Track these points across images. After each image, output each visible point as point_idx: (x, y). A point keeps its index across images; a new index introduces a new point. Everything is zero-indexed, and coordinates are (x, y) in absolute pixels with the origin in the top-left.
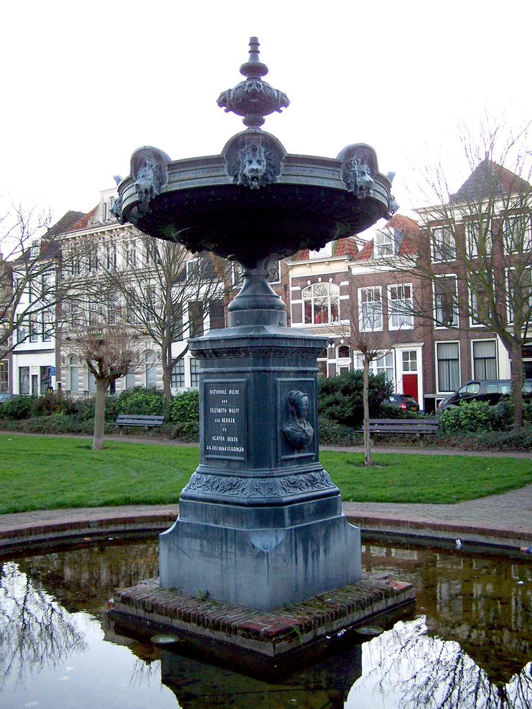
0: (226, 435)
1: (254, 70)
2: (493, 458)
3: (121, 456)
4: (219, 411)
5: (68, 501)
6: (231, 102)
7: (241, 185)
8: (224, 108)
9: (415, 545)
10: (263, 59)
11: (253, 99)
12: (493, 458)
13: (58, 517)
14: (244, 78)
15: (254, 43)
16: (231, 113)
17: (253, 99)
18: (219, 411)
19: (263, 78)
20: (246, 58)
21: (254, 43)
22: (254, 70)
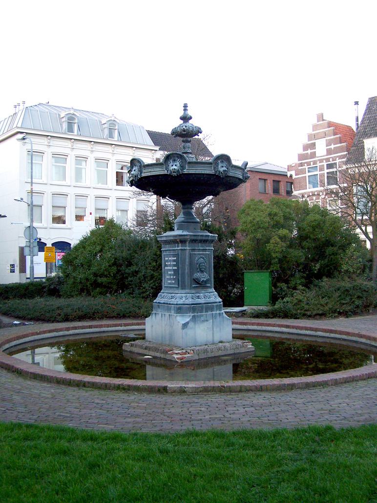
1: (186, 118)
7: (170, 175)
10: (190, 113)
14: (182, 122)
15: (185, 106)
19: (190, 121)
20: (181, 113)
21: (185, 106)
22: (186, 118)
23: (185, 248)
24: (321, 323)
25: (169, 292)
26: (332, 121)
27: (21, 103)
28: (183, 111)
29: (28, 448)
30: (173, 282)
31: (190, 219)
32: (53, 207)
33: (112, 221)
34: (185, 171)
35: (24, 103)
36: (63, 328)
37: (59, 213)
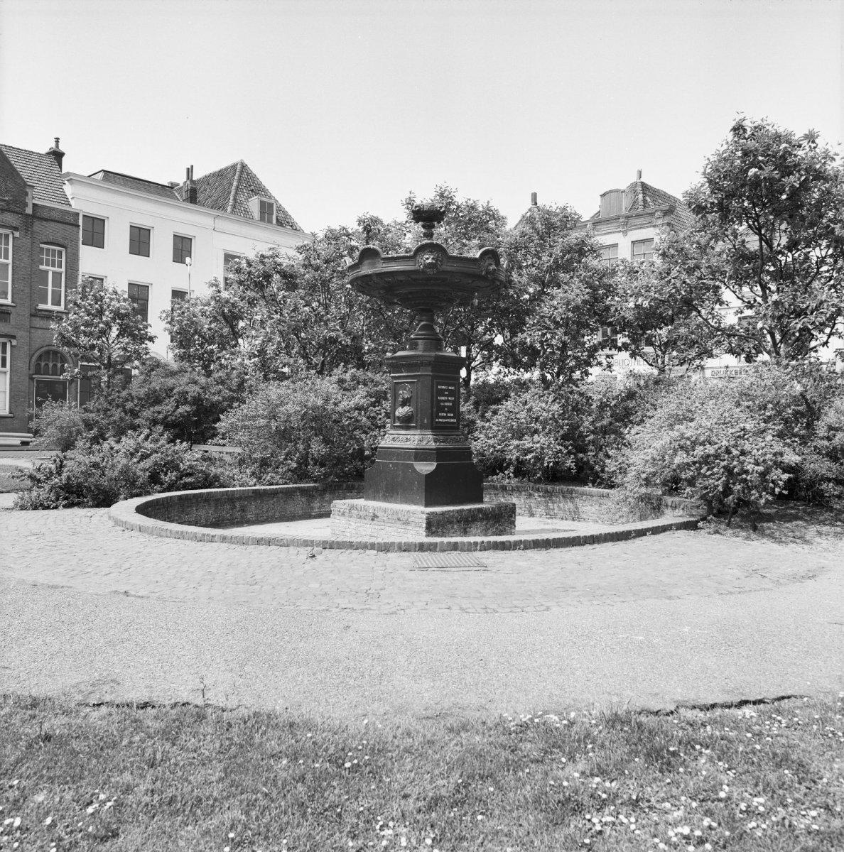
0: (447, 412)
4: (443, 398)
18: (443, 398)
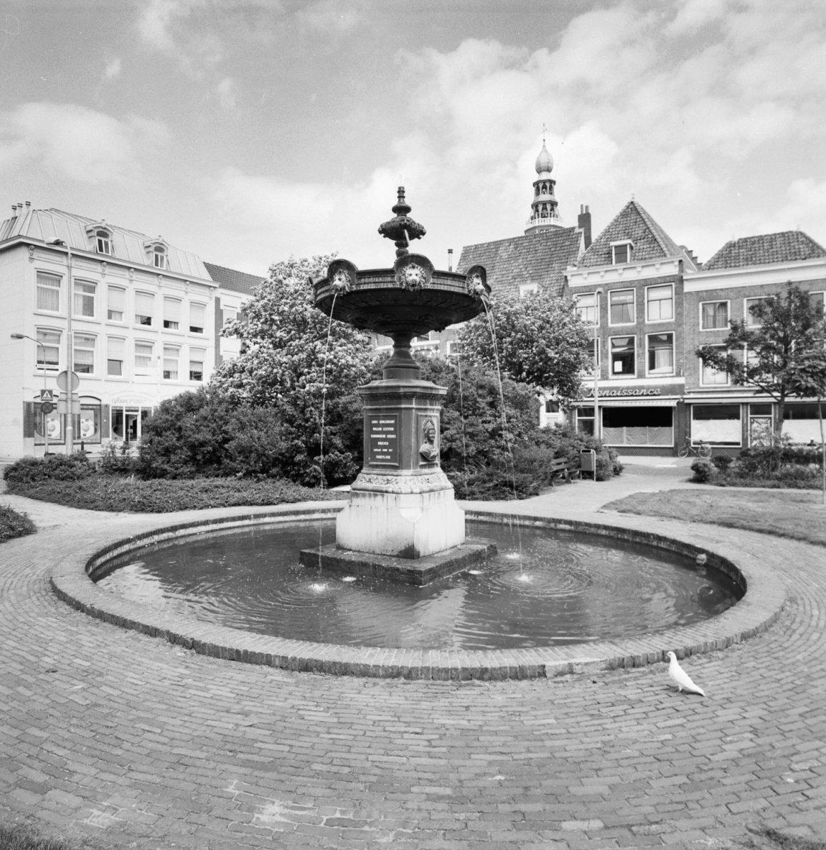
1: (401, 210)
2: (541, 405)
3: (231, 751)
5: (511, 685)
6: (396, 210)
7: (405, 289)
8: (383, 235)
9: (324, 671)
10: (408, 202)
11: (401, 230)
12: (541, 405)
13: (377, 373)
14: (395, 215)
15: (401, 192)
16: (387, 239)
17: (401, 230)
19: (408, 215)
20: (395, 202)
21: (401, 192)
22: (401, 210)
23: (410, 406)
24: (710, 493)
25: (383, 472)
26: (22, 432)
27: (24, 204)
28: (397, 199)
29: (261, 347)
30: (389, 457)
31: (408, 362)
32: (191, 362)
33: (277, 636)
34: (429, 286)
35: (28, 204)
36: (139, 624)
37: (196, 369)
